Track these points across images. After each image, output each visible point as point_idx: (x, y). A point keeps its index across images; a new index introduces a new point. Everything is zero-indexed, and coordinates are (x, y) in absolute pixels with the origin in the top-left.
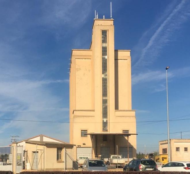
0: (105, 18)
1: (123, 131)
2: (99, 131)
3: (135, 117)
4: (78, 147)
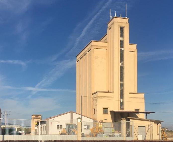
0: (122, 17)
1: (135, 109)
2: (117, 109)
3: (144, 99)
4: (101, 122)
